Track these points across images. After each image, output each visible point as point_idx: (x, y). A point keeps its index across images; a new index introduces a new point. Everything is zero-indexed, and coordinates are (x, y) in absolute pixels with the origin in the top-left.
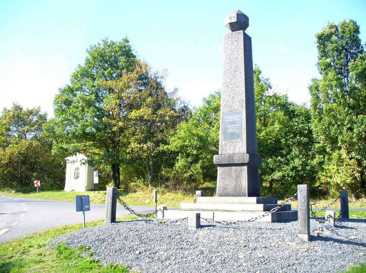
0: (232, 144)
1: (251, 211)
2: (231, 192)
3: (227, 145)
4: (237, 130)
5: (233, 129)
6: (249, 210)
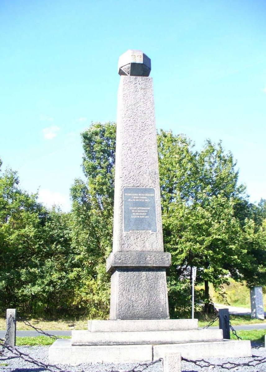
0: (139, 236)
1: (203, 341)
2: (142, 312)
3: (132, 238)
4: (147, 215)
5: (141, 214)
6: (200, 339)
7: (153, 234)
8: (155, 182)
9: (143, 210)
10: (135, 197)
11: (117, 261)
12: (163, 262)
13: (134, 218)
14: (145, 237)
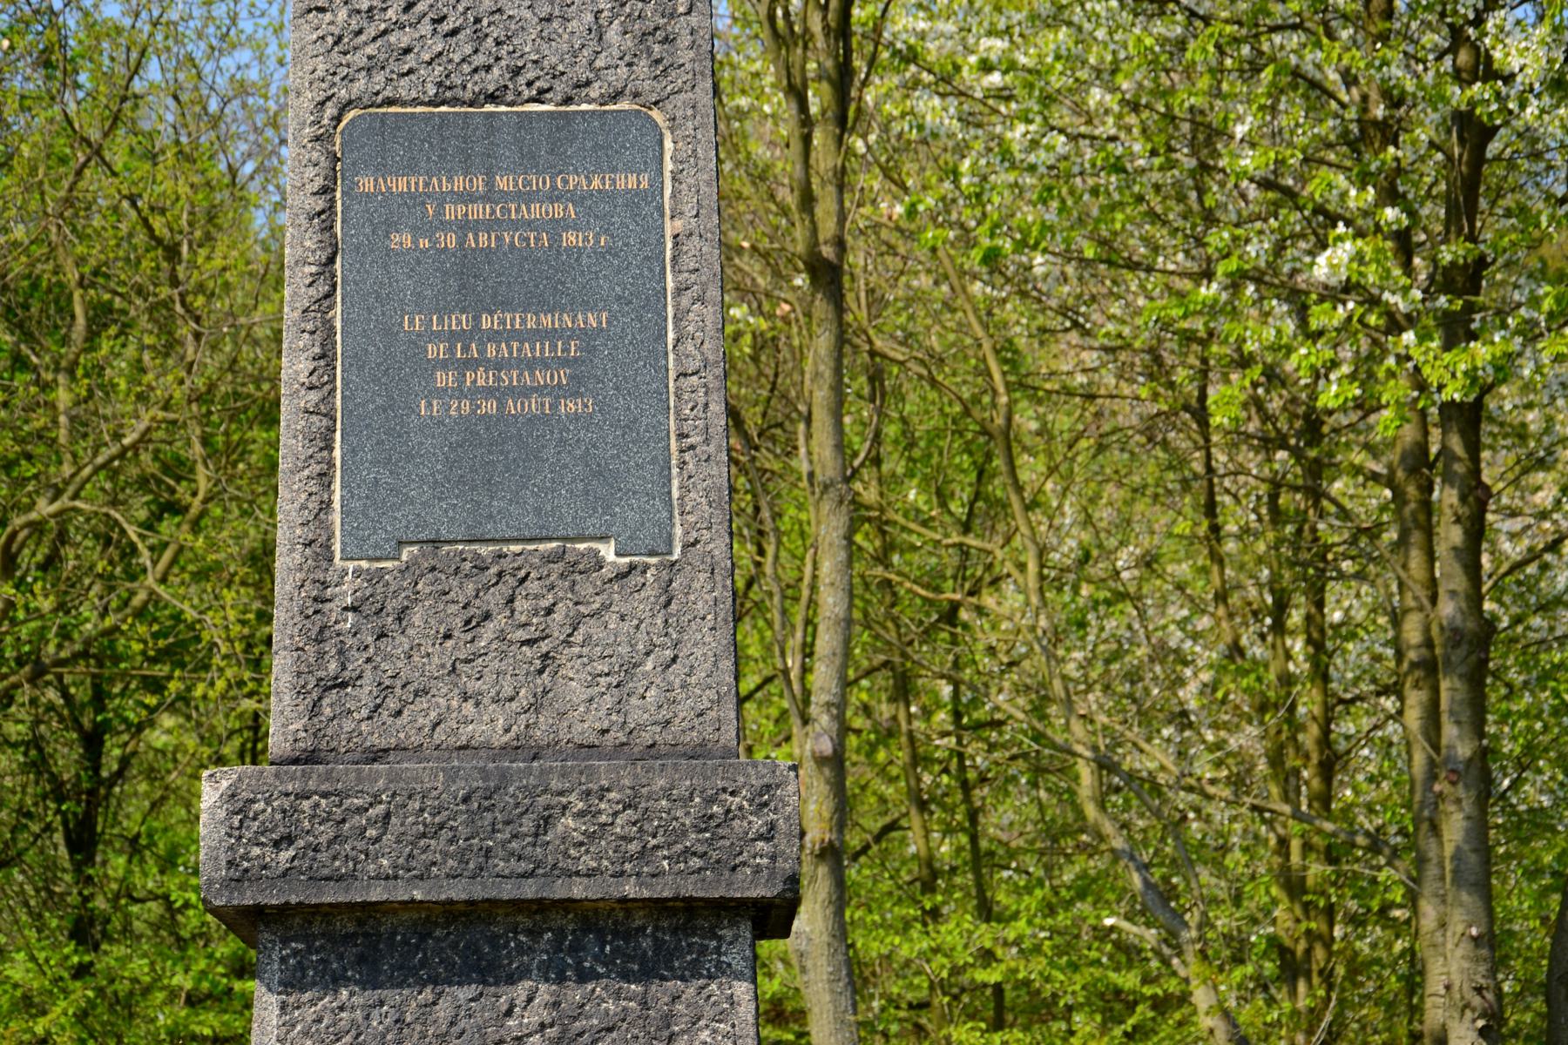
0: (494, 599)
5: (510, 378)
7: (635, 579)
8: (666, 40)
9: (540, 334)
10: (452, 212)
11: (256, 851)
12: (715, 855)
13: (441, 423)
14: (549, 611)
